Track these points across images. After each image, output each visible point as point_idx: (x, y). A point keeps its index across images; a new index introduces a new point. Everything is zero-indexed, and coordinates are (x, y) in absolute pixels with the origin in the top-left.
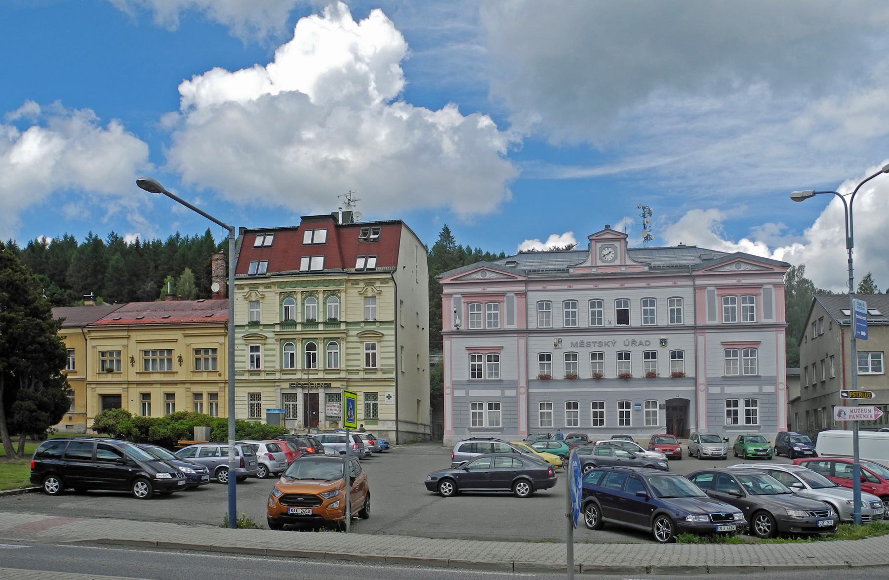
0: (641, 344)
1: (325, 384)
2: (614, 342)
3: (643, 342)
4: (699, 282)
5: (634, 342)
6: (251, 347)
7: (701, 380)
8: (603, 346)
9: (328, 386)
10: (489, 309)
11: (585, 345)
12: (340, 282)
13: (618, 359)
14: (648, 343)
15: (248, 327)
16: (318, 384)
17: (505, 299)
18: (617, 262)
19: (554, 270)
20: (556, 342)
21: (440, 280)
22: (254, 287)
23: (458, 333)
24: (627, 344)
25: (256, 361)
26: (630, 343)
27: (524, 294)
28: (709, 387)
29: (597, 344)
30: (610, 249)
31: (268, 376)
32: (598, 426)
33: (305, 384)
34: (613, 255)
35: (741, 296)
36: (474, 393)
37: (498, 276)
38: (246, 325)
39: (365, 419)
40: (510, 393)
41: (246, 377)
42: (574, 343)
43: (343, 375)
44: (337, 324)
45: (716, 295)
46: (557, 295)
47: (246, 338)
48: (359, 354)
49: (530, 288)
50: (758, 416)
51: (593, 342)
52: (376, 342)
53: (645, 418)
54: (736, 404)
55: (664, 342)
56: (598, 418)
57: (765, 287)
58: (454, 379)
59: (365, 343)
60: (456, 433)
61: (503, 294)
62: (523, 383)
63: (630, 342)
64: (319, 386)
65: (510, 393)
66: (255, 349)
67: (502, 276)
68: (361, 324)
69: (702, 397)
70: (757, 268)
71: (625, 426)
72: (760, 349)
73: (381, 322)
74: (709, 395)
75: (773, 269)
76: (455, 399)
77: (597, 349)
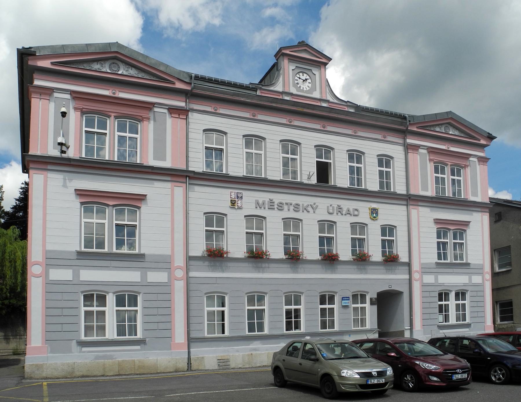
0: (348, 213)
2: (314, 206)
3: (351, 210)
4: (410, 141)
5: (271, 205)
7: (416, 266)
8: (301, 211)
10: (453, 174)
11: (276, 206)
13: (206, 227)
14: (356, 213)
17: (151, 115)
20: (233, 196)
21: (30, 58)
24: (331, 211)
28: (51, 270)
30: (305, 75)
32: (127, 337)
34: (310, 85)
40: (155, 277)
42: (261, 202)
51: (287, 204)
54: (102, 300)
55: (374, 212)
56: (293, 320)
58: (423, 261)
60: (52, 351)
62: (180, 261)
63: (335, 209)
65: (155, 277)
70: (457, 133)
71: (461, 322)
72: (145, 209)
74: (424, 285)
77: (292, 214)
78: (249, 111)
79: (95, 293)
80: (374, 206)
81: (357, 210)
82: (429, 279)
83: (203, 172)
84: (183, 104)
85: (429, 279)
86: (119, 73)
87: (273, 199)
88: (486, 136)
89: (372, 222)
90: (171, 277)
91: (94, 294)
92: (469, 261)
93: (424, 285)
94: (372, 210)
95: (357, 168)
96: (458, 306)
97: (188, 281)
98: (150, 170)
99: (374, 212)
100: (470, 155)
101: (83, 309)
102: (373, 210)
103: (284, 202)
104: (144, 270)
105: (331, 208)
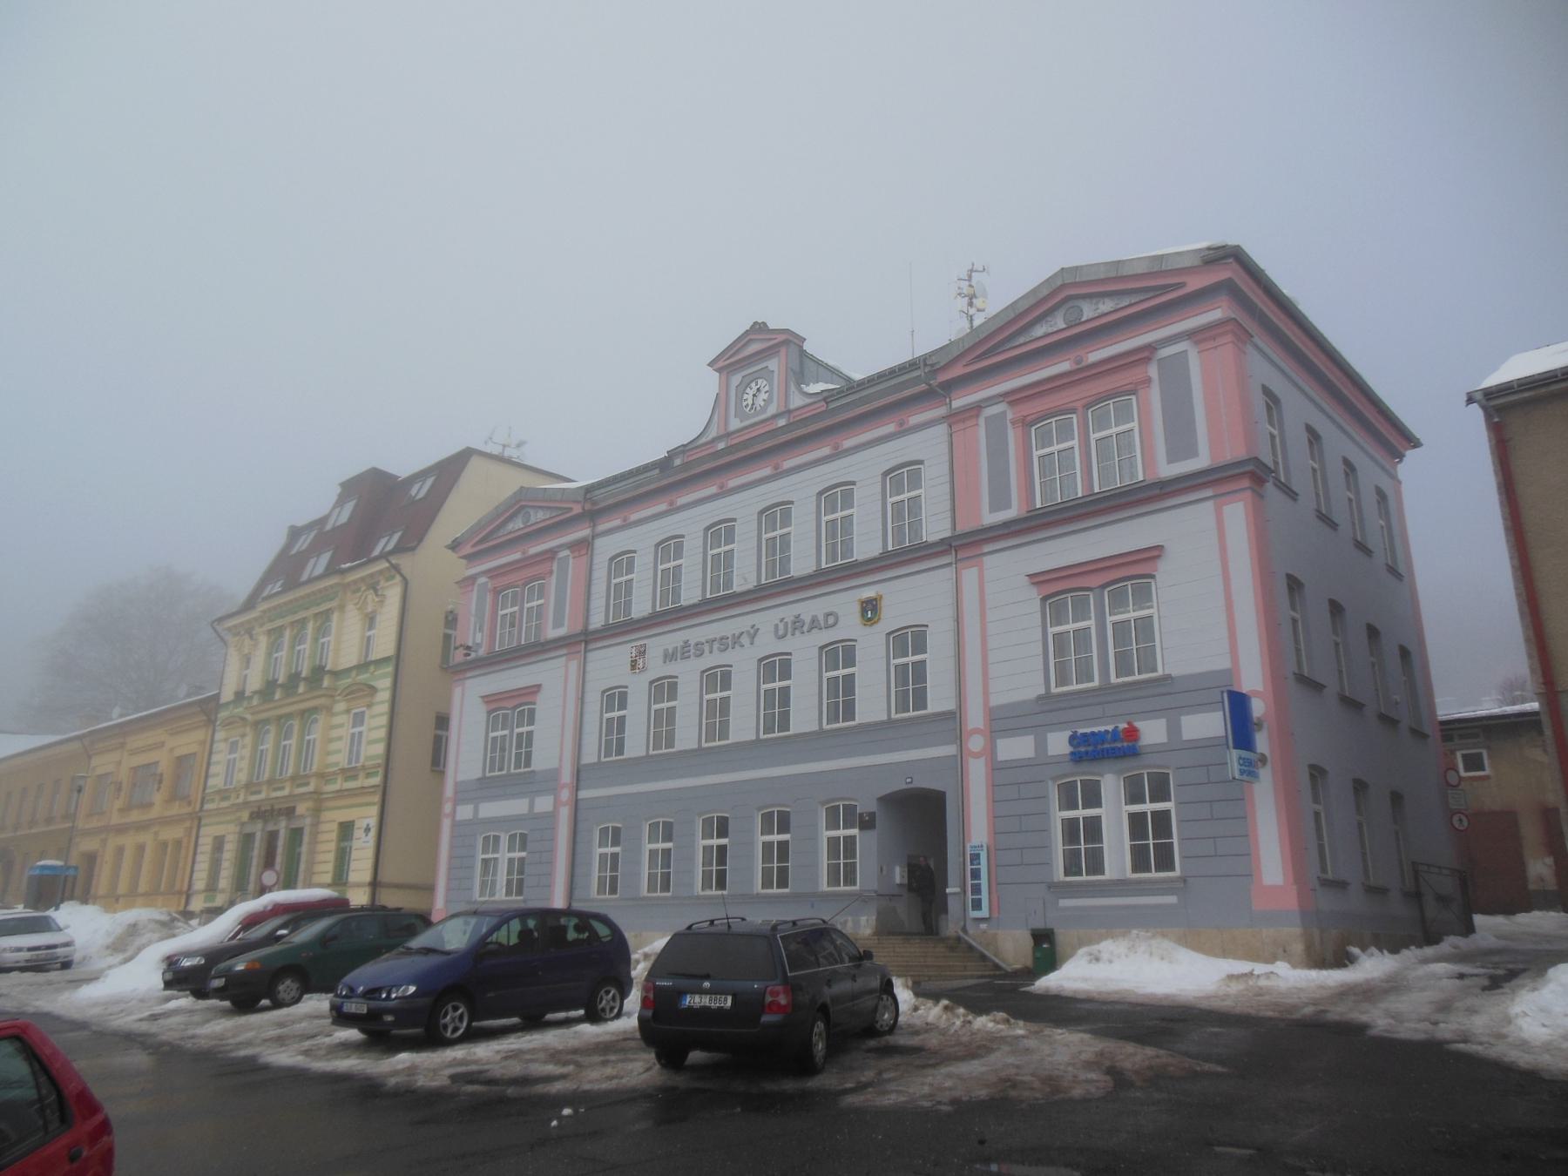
0: (814, 624)
3: (821, 618)
7: (975, 717)
17: (1153, 371)
19: (868, 381)
20: (634, 655)
26: (790, 630)
29: (716, 645)
36: (489, 810)
40: (544, 804)
52: (364, 709)
53: (858, 861)
55: (870, 609)
57: (1165, 352)
58: (995, 701)
61: (551, 555)
62: (567, 777)
65: (544, 804)
69: (977, 772)
71: (1154, 875)
72: (1165, 572)
75: (1181, 285)
77: (709, 661)
78: (1216, 305)
79: (841, 803)
80: (869, 593)
82: (1016, 748)
83: (1029, 514)
85: (1016, 748)
86: (1083, 320)
87: (799, 615)
89: (868, 630)
90: (991, 750)
91: (1143, 773)
94: (864, 605)
97: (576, 805)
99: (870, 609)
101: (1059, 815)
102: (872, 604)
103: (703, 640)
104: (1172, 714)
105: (781, 626)
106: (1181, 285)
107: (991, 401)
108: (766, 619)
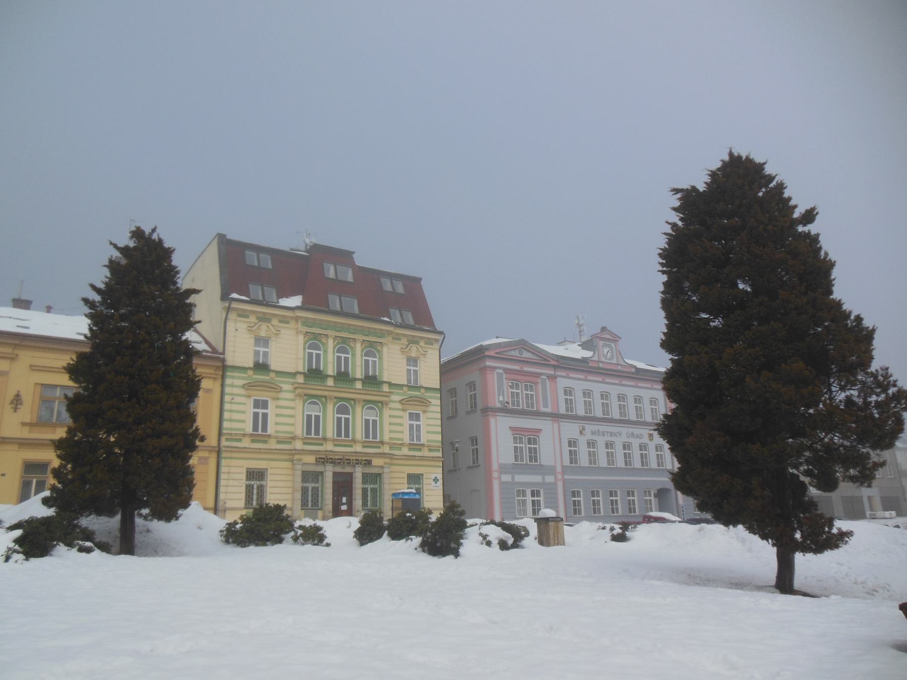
1: (365, 460)
5: (633, 435)
6: (409, 413)
9: (369, 463)
12: (382, 334)
15: (274, 374)
16: (356, 460)
17: (540, 380)
18: (614, 361)
22: (264, 319)
23: (505, 410)
25: (260, 422)
27: (553, 378)
31: (364, 449)
33: (339, 459)
34: (610, 354)
35: (524, 383)
36: (520, 478)
37: (538, 358)
38: (250, 368)
39: (245, 508)
40: (550, 479)
41: (246, 443)
43: (386, 449)
44: (377, 384)
45: (504, 378)
46: (578, 384)
47: (248, 387)
48: (402, 425)
49: (558, 373)
50: (601, 507)
51: (606, 432)
54: (524, 493)
58: (501, 461)
59: (408, 411)
62: (559, 469)
64: (358, 462)
65: (550, 479)
66: (258, 404)
67: (535, 357)
68: (421, 389)
70: (538, 358)
73: (426, 388)
76: (502, 484)
77: (609, 438)
81: (642, 435)
82: (506, 478)
84: (552, 372)
85: (506, 478)
88: (105, 282)
92: (542, 464)
93: (502, 484)
95: (570, 399)
96: (533, 502)
97: (564, 480)
98: (532, 414)
100: (541, 374)
101: (541, 499)
106: (550, 361)
107: (500, 368)
108: (625, 430)
